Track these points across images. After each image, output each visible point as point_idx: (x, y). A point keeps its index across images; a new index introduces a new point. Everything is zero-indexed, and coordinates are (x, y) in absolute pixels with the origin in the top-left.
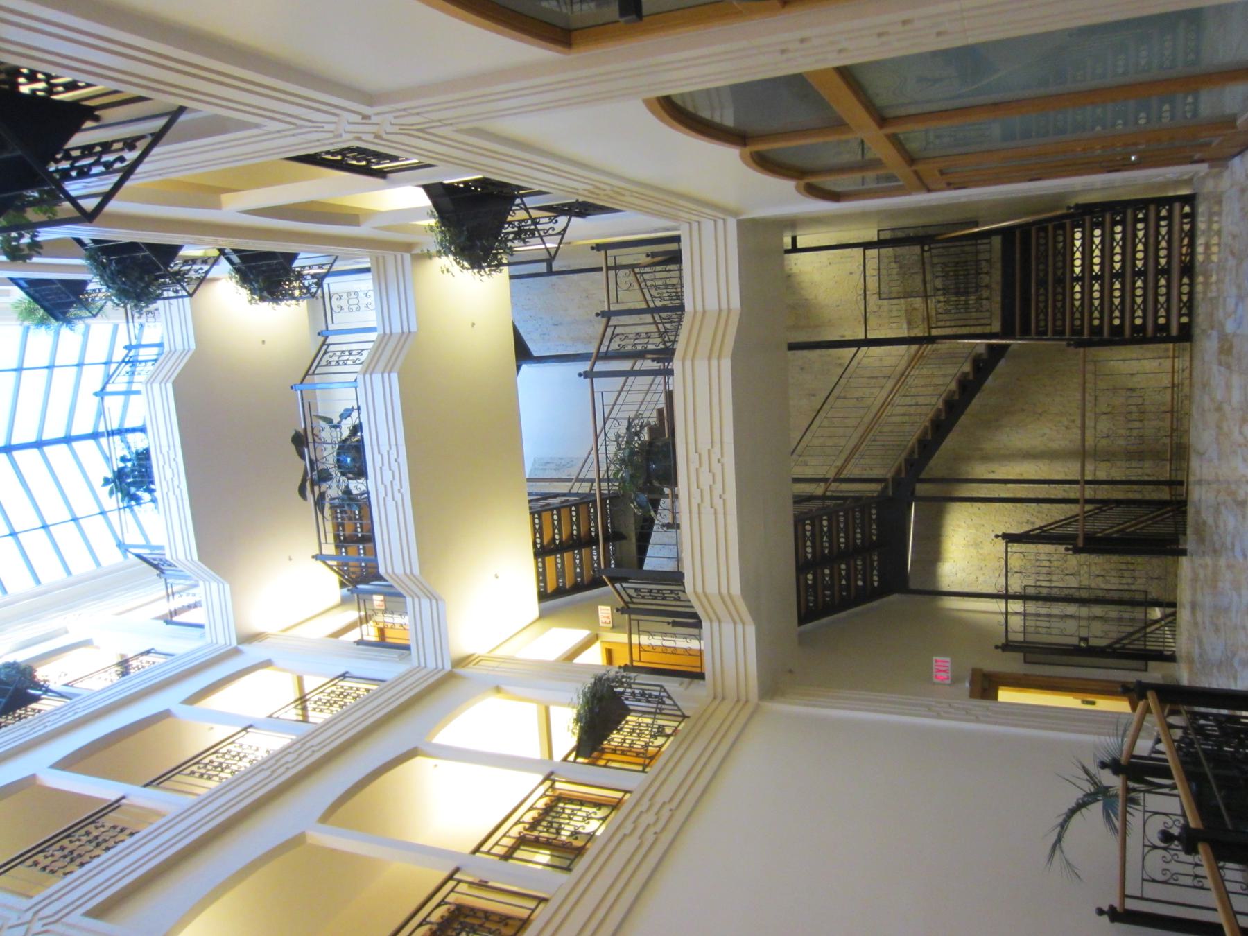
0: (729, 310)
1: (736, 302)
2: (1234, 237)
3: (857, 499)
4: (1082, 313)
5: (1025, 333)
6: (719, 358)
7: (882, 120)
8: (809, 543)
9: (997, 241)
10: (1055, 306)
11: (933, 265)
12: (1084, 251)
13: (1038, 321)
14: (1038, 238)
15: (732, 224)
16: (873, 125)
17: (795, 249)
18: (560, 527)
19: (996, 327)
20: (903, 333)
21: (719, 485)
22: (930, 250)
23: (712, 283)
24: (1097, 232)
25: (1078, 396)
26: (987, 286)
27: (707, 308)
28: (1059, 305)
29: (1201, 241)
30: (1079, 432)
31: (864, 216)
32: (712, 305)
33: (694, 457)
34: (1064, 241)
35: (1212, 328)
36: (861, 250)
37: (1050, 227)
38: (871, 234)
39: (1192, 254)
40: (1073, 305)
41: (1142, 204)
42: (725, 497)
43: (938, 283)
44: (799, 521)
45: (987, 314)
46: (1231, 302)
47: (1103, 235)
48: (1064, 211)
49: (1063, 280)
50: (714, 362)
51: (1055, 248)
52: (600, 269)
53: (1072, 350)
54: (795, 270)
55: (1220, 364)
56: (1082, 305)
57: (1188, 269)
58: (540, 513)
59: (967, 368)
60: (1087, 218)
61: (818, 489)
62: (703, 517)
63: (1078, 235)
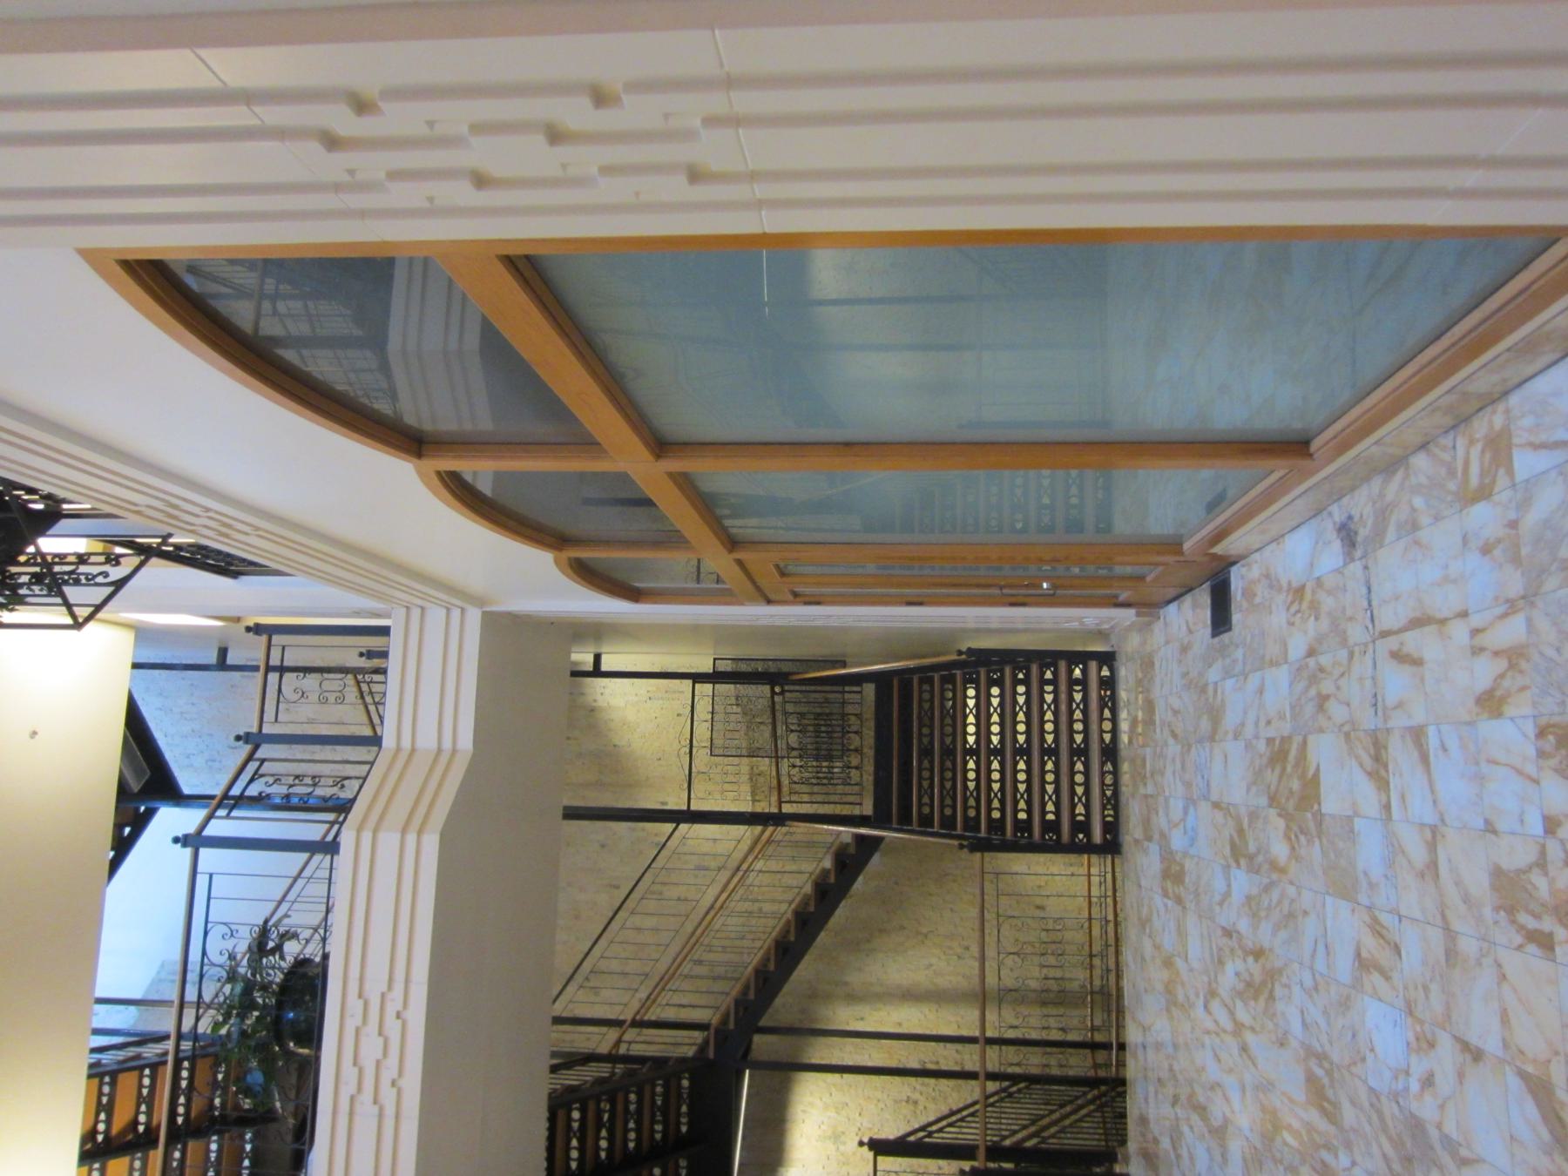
0: (454, 751)
1: (466, 742)
2: (1176, 712)
3: (659, 1062)
4: (978, 800)
5: (905, 820)
6: (420, 832)
7: (661, 446)
8: (574, 1143)
9: (869, 689)
10: (942, 786)
11: (785, 713)
12: (978, 715)
13: (920, 805)
14: (921, 692)
15: (474, 617)
16: (645, 454)
17: (597, 672)
18: (150, 1101)
19: (868, 809)
20: (745, 807)
21: (392, 1061)
22: (782, 693)
23: (434, 706)
24: (995, 691)
25: (974, 912)
26: (856, 750)
27: (420, 744)
28: (948, 785)
29: (1123, 715)
30: (976, 964)
31: (694, 632)
32: (427, 740)
33: (355, 1005)
34: (954, 698)
35: (1149, 839)
36: (689, 683)
37: (936, 677)
38: (706, 666)
39: (1115, 731)
40: (966, 787)
41: (1048, 658)
42: (402, 1083)
43: (793, 739)
44: (558, 1105)
45: (856, 788)
46: (1177, 806)
47: (1002, 695)
48: (954, 657)
49: (952, 752)
50: (411, 838)
51: (942, 706)
52: (256, 668)
53: (965, 853)
54: (601, 702)
55: (1165, 894)
56: (978, 787)
57: (1111, 752)
58: (114, 1074)
59: (828, 863)
60: (983, 671)
61: (602, 1040)
62: (358, 1120)
63: (971, 692)
